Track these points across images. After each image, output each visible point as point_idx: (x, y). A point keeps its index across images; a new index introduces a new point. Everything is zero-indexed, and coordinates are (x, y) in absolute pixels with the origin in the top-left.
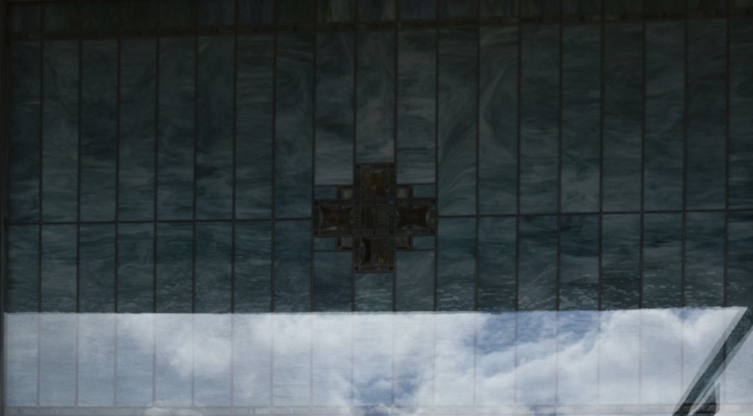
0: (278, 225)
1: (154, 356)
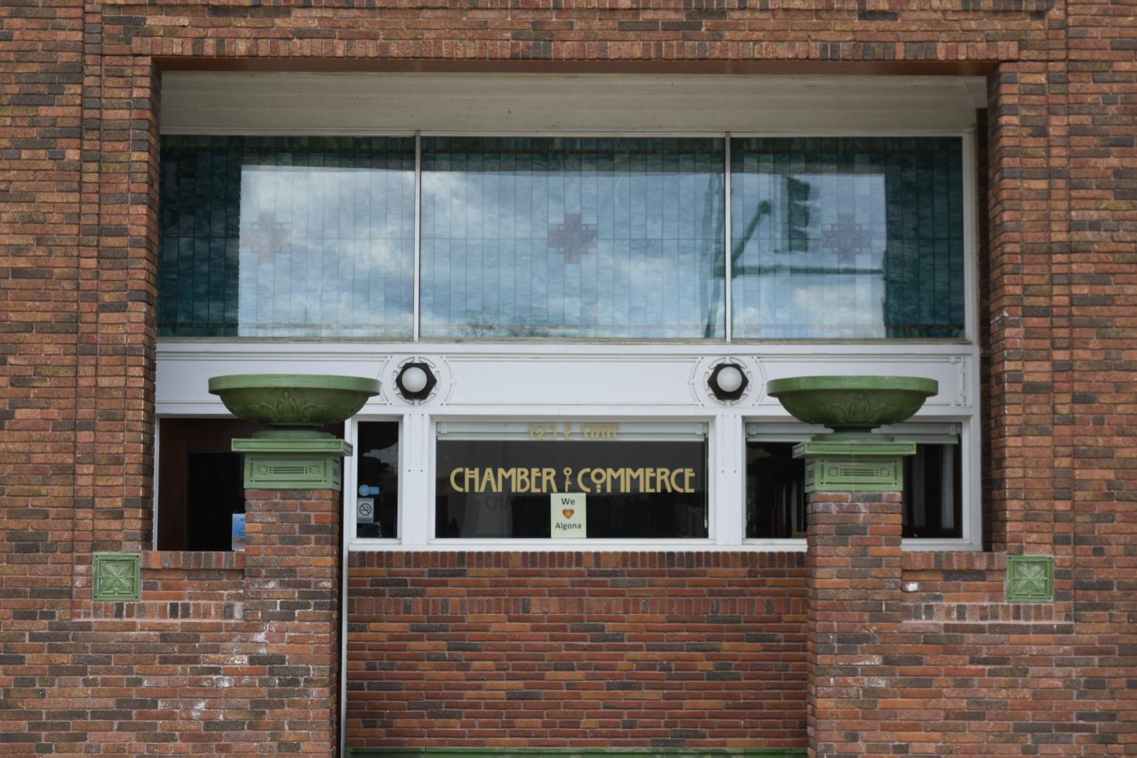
0: (534, 241)
1: (564, 316)
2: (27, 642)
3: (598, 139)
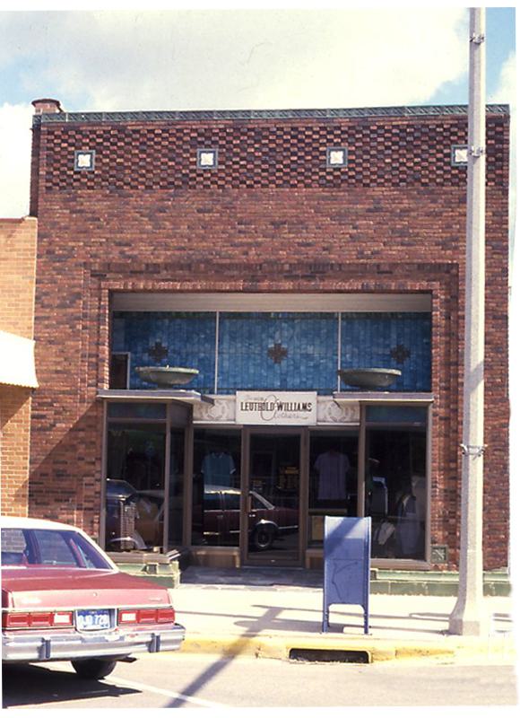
2: (129, 354)
3: (289, 313)
